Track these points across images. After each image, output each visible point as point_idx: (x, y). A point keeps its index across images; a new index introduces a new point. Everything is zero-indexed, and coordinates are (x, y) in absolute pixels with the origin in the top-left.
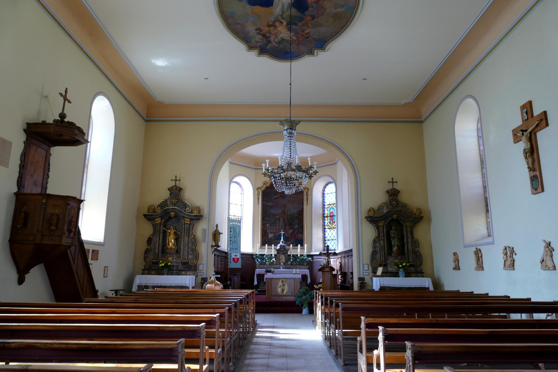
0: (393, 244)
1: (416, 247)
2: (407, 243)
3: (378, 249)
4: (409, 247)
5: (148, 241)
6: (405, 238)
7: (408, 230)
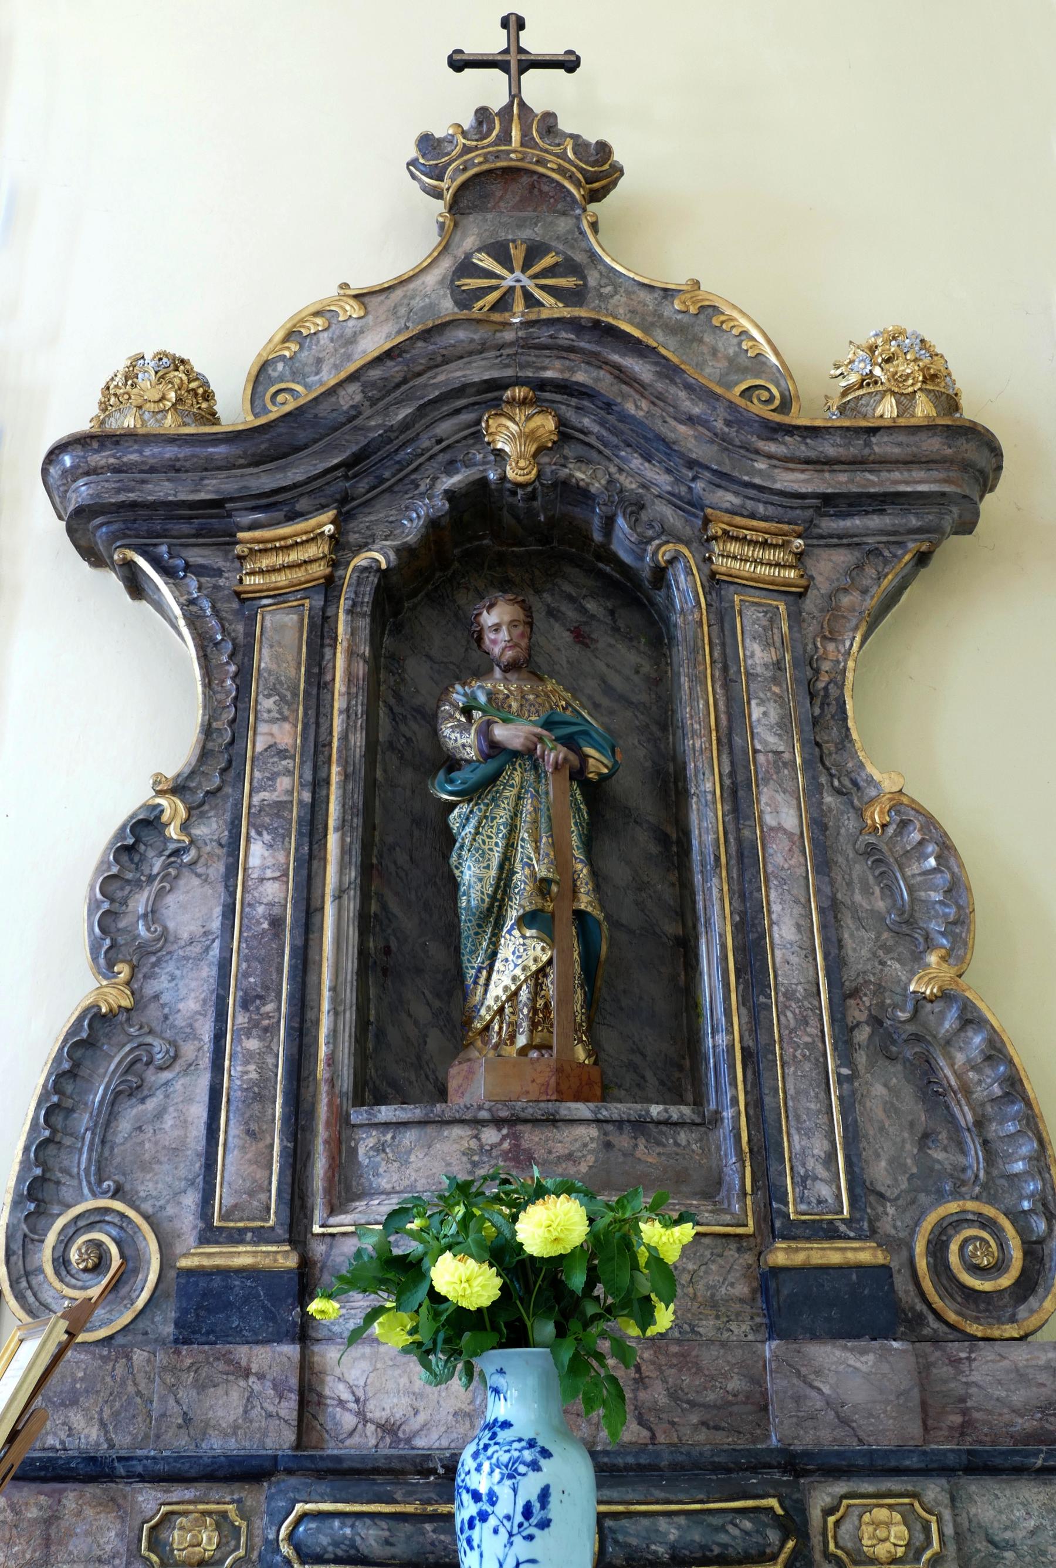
0: (473, 876)
1: (908, 933)
2: (745, 860)
3: (185, 993)
4: (784, 930)
6: (707, 784)
7: (756, 655)
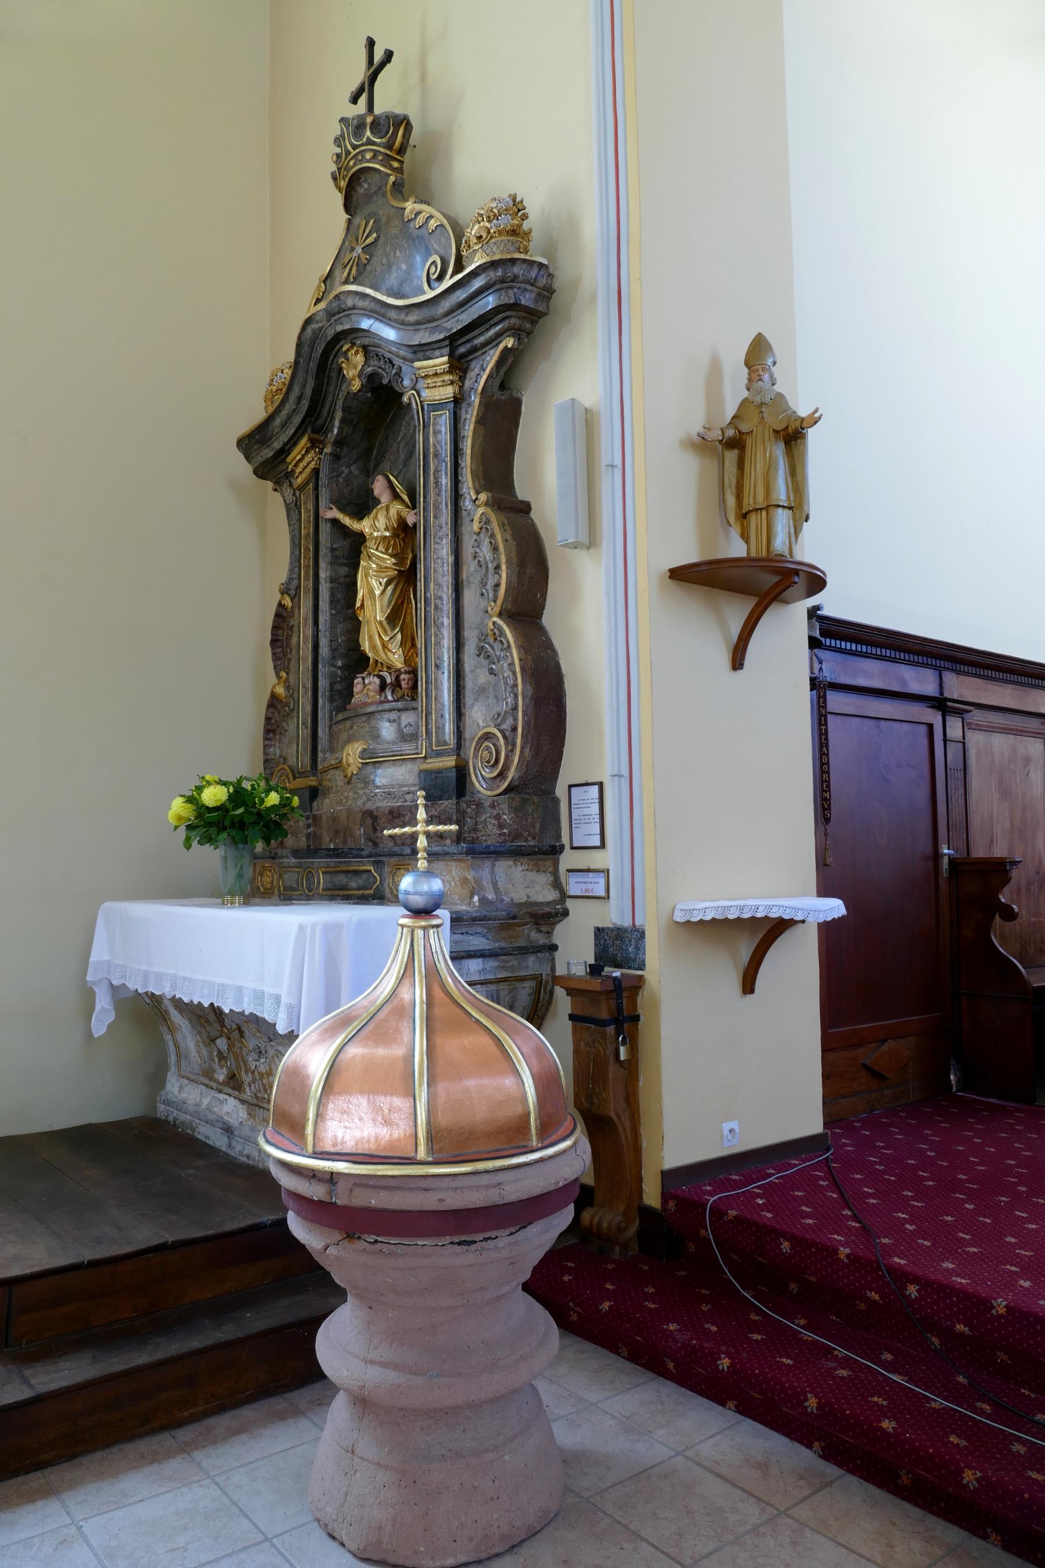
5: (274, 642)
